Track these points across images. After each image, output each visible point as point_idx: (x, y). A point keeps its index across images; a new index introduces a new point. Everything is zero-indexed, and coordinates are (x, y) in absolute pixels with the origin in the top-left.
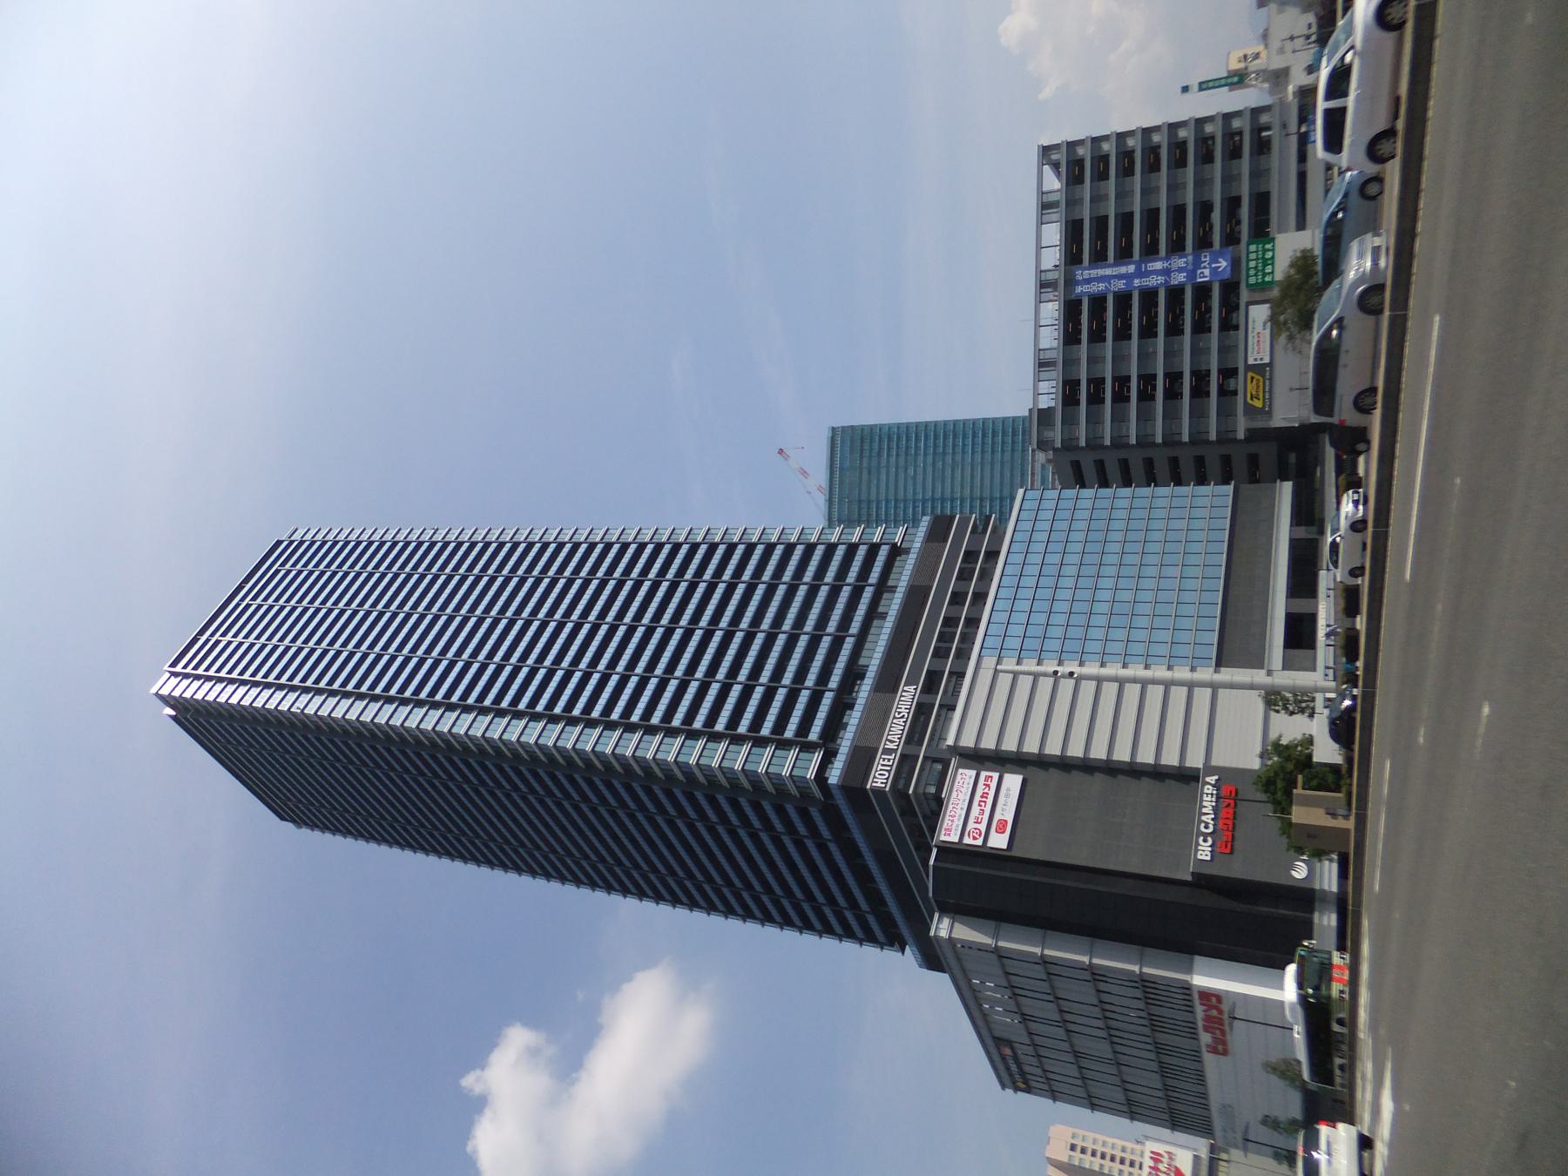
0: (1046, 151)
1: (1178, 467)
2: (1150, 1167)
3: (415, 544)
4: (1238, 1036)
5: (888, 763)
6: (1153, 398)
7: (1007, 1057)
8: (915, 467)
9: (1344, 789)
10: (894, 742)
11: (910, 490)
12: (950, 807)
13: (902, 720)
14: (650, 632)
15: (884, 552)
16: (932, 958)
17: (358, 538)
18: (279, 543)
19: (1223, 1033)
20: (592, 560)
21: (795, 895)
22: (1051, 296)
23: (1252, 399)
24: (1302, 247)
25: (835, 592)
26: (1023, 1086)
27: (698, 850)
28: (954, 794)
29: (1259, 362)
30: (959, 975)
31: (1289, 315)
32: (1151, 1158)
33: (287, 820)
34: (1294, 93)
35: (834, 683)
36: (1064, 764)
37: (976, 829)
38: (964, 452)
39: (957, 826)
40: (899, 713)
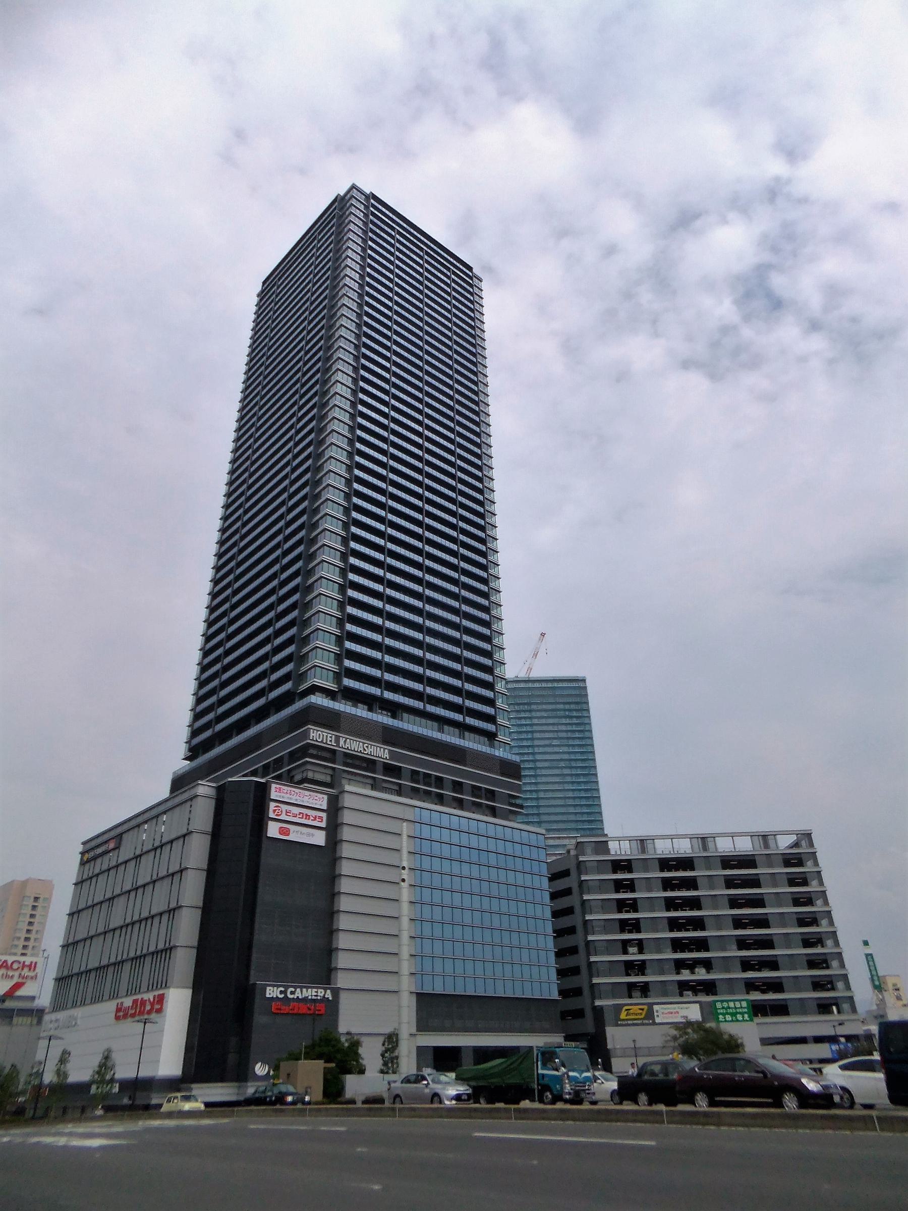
0: (808, 836)
1: (568, 934)
2: (24, 962)
3: (478, 420)
4: (132, 1027)
5: (328, 741)
6: (622, 931)
7: (107, 845)
8: (558, 746)
9: (325, 1100)
10: (345, 745)
11: (538, 714)
12: (297, 791)
13: (362, 749)
14: (419, 537)
15: (491, 727)
16: (180, 783)
17: (476, 293)
18: (470, 269)
19: (133, 1015)
20: (471, 492)
21: (232, 611)
22: (696, 846)
23: (626, 1010)
24: (745, 1043)
25: (457, 691)
26: (85, 859)
27: (281, 366)
28: (307, 793)
29: (655, 1014)
30: (169, 804)
31: (693, 1036)
32: (32, 962)
33: (263, 286)
34: (869, 1030)
35: (388, 695)
36: (333, 878)
37: (282, 811)
38: (573, 783)
39: (283, 797)
40: (367, 747)
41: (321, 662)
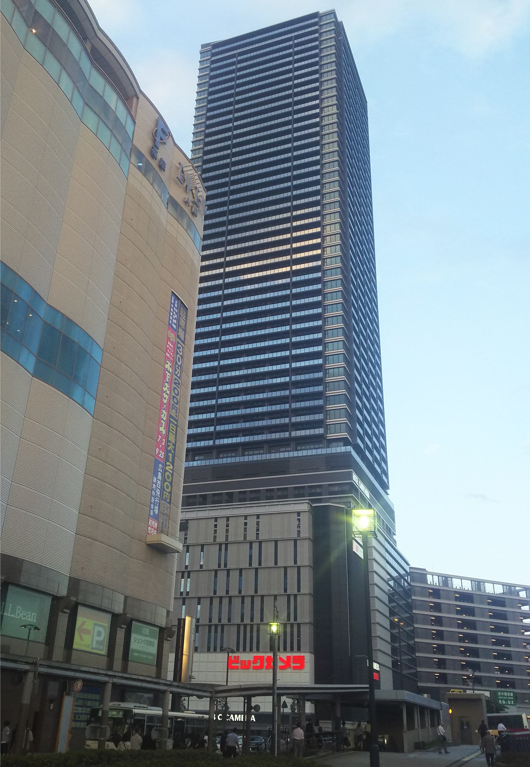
41: (335, 265)
